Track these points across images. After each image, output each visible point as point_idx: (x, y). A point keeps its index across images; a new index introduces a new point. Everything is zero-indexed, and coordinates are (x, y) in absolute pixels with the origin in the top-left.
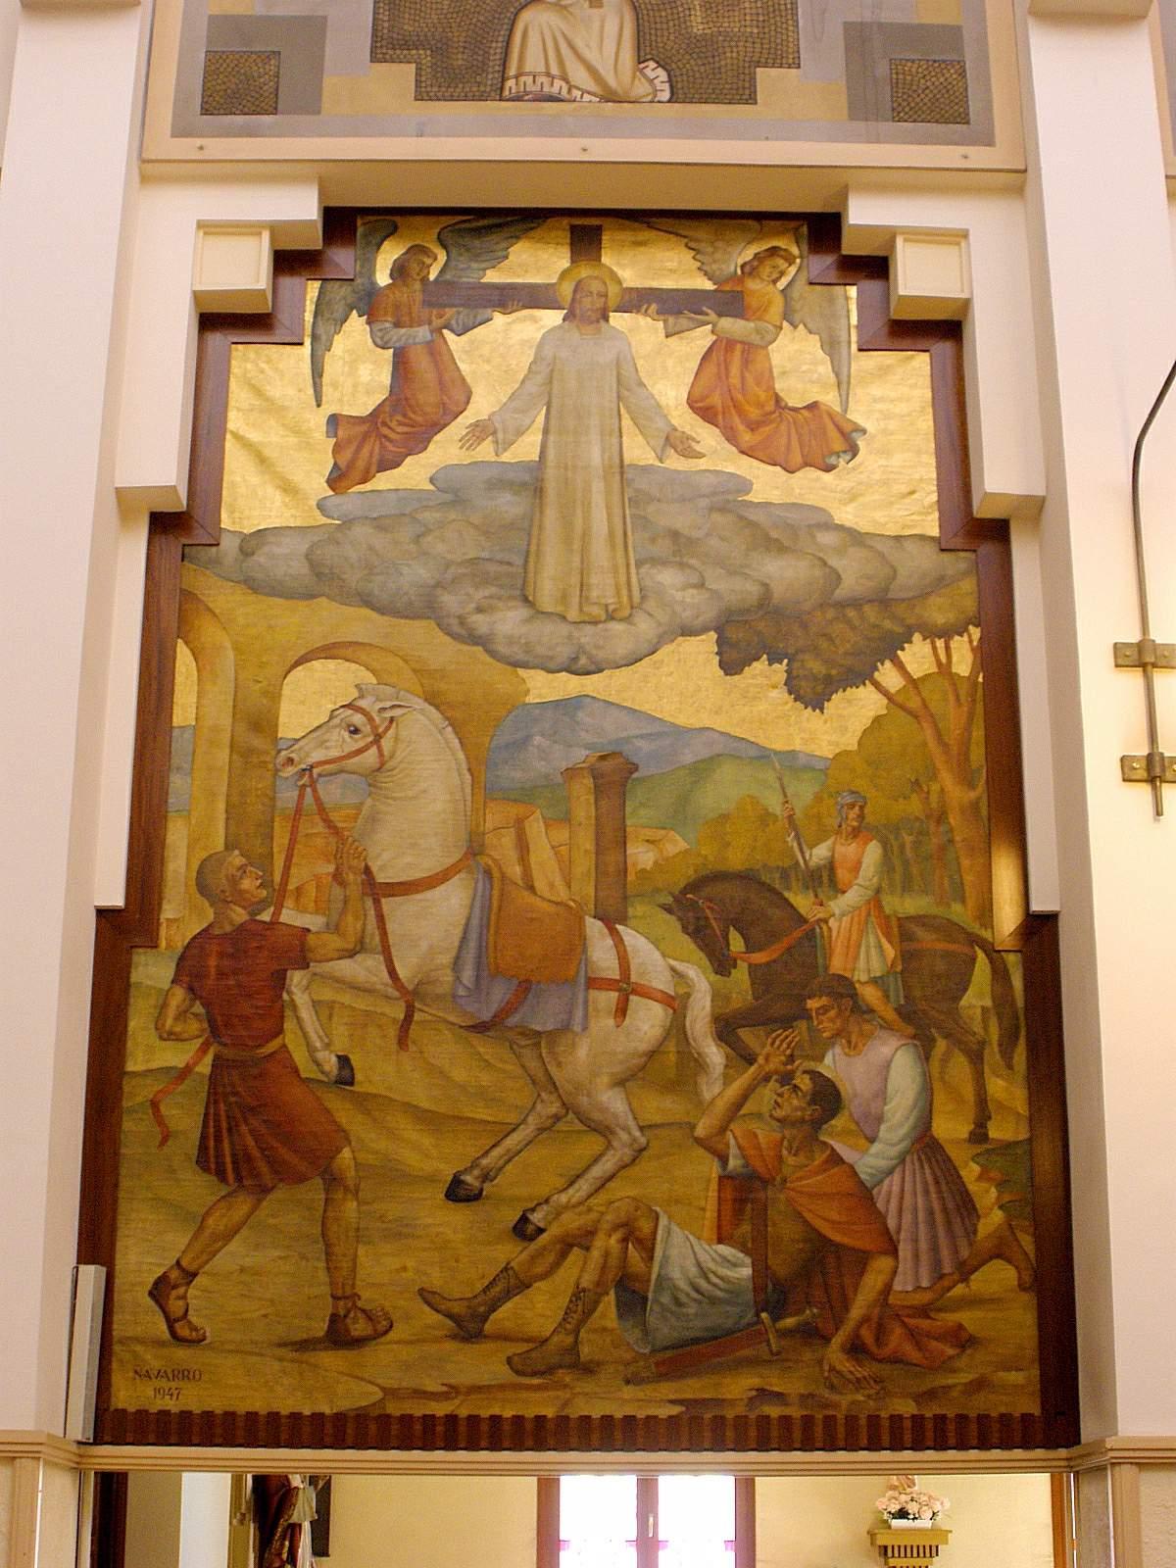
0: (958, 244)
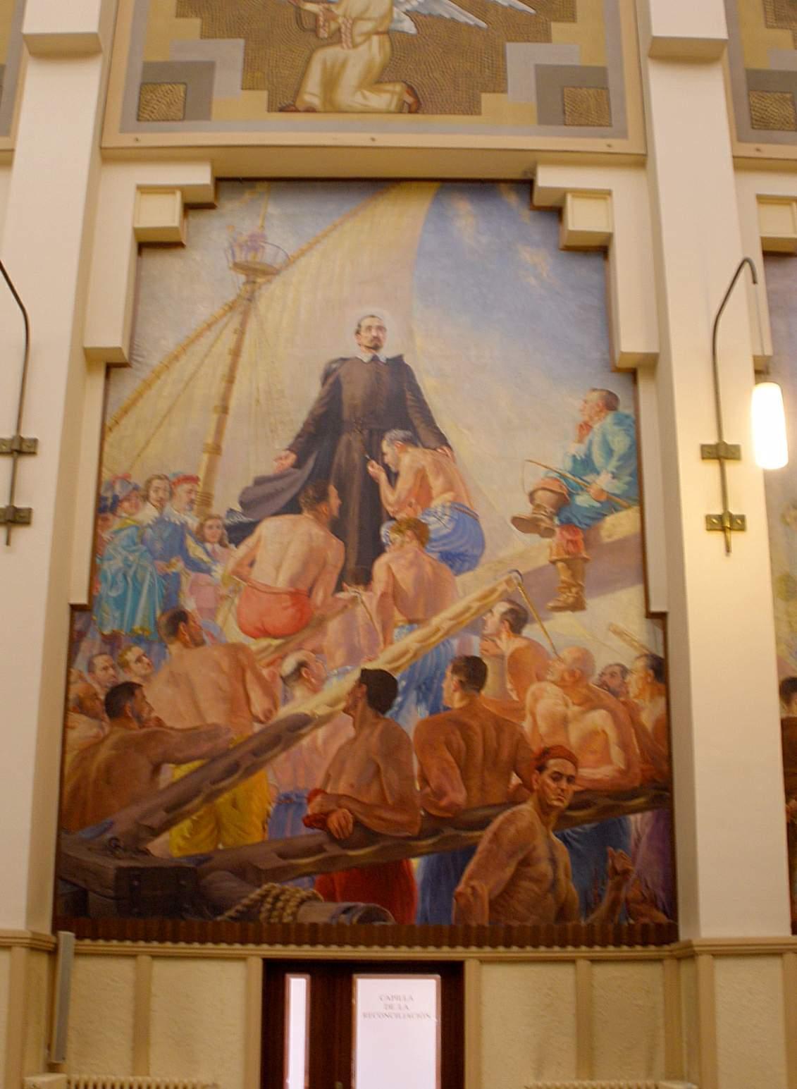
0: (605, 199)
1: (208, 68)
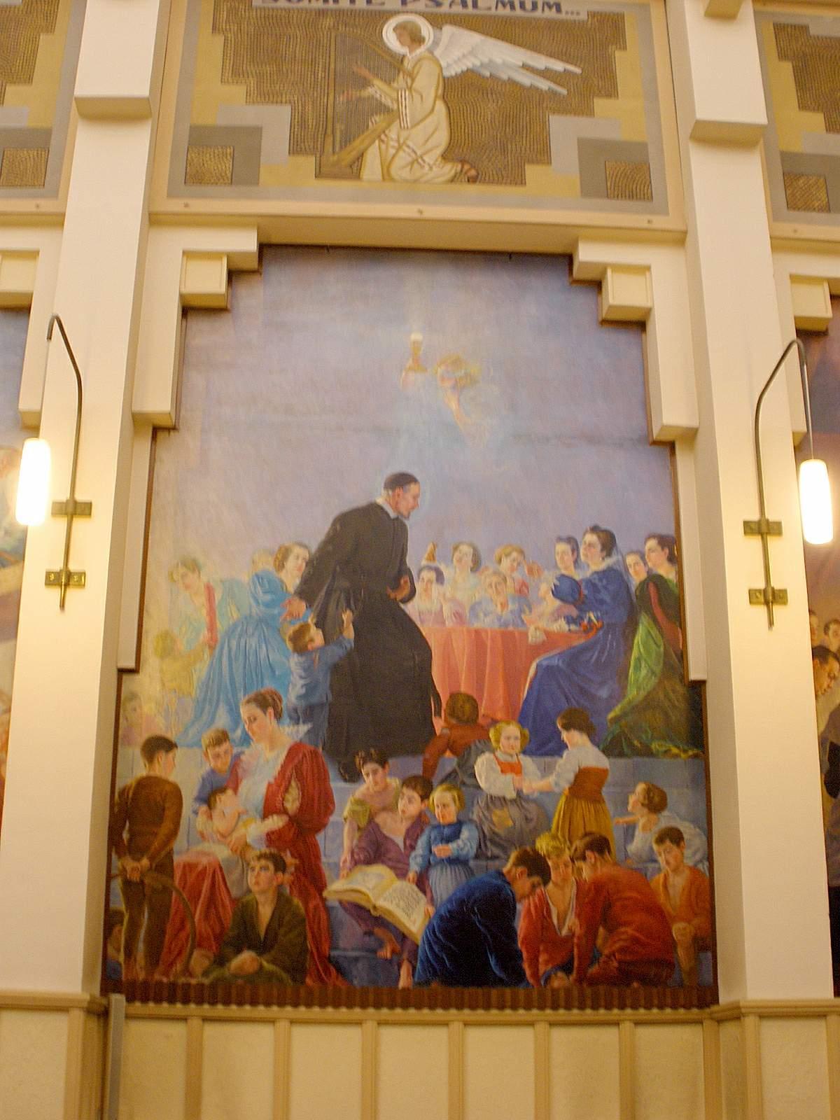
0: (644, 274)
1: (255, 133)
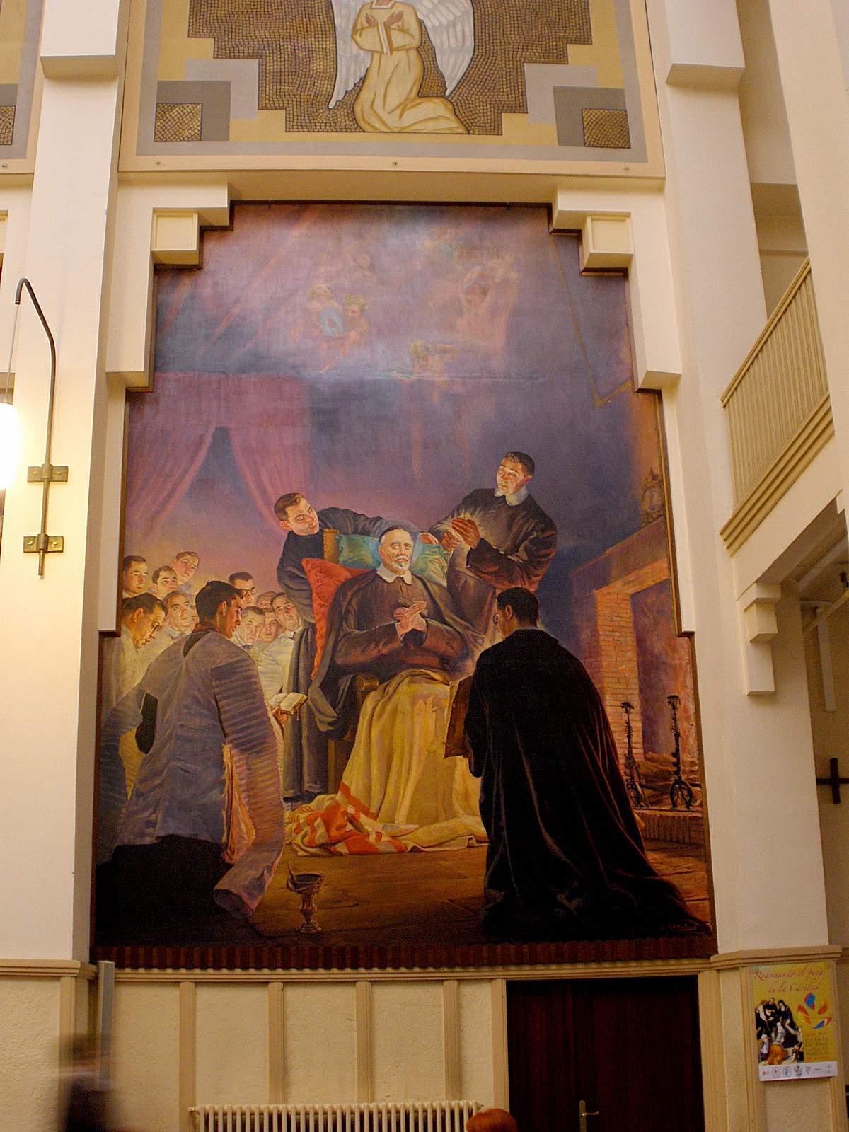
1: (222, 90)
